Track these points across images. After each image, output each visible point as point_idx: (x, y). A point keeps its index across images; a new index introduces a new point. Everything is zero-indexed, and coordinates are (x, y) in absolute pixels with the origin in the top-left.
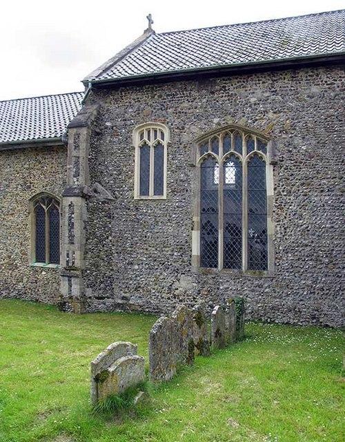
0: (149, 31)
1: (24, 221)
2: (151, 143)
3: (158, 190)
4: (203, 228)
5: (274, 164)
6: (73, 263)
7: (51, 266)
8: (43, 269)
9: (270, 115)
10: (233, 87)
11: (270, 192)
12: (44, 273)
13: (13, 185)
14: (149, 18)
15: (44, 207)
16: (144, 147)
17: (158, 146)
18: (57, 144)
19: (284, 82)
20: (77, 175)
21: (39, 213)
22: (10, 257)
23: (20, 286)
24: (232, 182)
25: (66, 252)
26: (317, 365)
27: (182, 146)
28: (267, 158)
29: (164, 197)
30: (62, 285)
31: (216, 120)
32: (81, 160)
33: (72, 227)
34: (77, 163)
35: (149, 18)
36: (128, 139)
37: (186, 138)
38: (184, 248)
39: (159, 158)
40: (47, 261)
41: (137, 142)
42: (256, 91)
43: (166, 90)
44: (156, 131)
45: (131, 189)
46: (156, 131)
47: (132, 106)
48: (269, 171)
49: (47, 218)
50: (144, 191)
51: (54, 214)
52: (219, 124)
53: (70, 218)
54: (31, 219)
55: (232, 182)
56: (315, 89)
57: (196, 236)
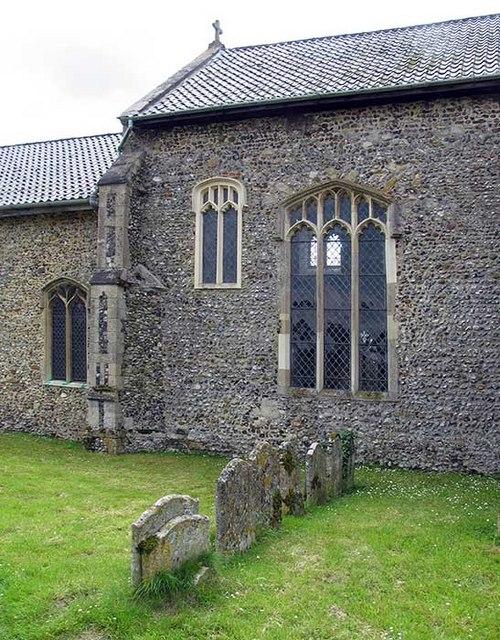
0: (216, 44)
1: (35, 320)
2: (219, 207)
3: (230, 276)
4: (294, 330)
5: (397, 237)
6: (106, 381)
7: (74, 385)
8: (62, 389)
9: (392, 166)
10: (338, 126)
11: (391, 278)
12: (63, 395)
13: (19, 268)
14: (216, 25)
15: (64, 299)
16: (209, 213)
17: (230, 212)
18: (82, 209)
19: (412, 119)
20: (111, 253)
21: (56, 308)
22: (14, 372)
23: (29, 413)
24: (337, 263)
25: (95, 366)
26: (460, 529)
27: (263, 212)
28: (387, 229)
29: (238, 285)
30: (90, 413)
31: (313, 174)
32: (117, 231)
33: (105, 329)
34: (111, 236)
35: (216, 25)
36: (186, 202)
37: (269, 199)
38: (267, 359)
39: (230, 228)
40: (68, 378)
41: (198, 206)
42: (371, 132)
43: (241, 130)
44: (225, 190)
45: (190, 273)
46: (225, 190)
47: (191, 154)
48: (390, 248)
49: (68, 316)
50: (209, 276)
51: (79, 310)
52: (317, 179)
53: (102, 316)
54: (44, 317)
55: (337, 263)
56: (456, 129)
57: (284, 341)
